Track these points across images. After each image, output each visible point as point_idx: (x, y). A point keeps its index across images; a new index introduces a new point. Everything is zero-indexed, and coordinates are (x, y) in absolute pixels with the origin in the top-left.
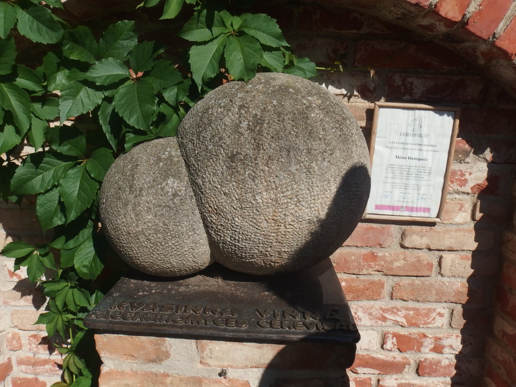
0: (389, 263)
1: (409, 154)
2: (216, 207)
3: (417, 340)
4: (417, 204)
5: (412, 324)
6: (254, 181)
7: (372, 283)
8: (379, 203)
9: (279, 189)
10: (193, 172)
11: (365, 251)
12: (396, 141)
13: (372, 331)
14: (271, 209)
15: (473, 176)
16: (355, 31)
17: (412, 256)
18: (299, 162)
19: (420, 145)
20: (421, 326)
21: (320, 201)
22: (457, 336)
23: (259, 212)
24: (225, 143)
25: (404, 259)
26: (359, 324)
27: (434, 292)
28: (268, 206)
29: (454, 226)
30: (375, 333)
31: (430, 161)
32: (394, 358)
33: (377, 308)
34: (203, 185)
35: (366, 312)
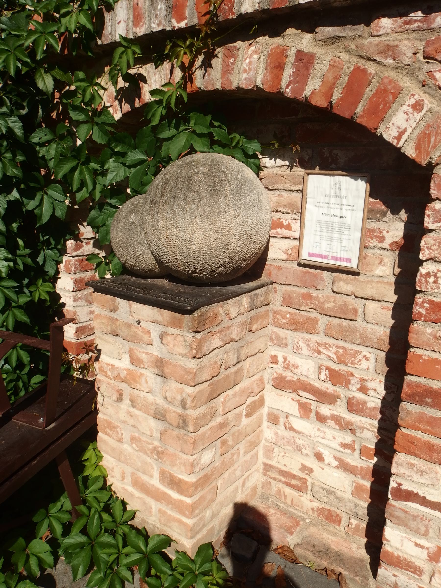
1: (332, 212)
3: (345, 377)
5: (340, 362)
7: (309, 318)
8: (311, 252)
15: (390, 234)
16: (294, 117)
18: (179, 204)
19: (341, 205)
20: (349, 365)
22: (380, 382)
25: (334, 302)
29: (376, 278)
31: (349, 218)
32: (327, 389)
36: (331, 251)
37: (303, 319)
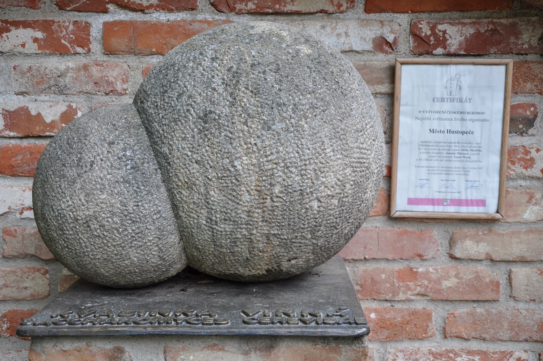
0: (435, 282)
2: (186, 180)
4: (466, 194)
6: (231, 144)
7: (414, 313)
8: (412, 196)
9: (262, 152)
11: (398, 266)
12: (428, 109)
14: (253, 177)
17: (467, 272)
19: (462, 113)
21: (313, 166)
23: (238, 181)
24: (195, 102)
25: (456, 276)
27: (506, 325)
28: (249, 173)
29: (524, 226)
31: (477, 133)
33: (425, 352)
34: (170, 154)
36: (449, 190)
37: (403, 317)
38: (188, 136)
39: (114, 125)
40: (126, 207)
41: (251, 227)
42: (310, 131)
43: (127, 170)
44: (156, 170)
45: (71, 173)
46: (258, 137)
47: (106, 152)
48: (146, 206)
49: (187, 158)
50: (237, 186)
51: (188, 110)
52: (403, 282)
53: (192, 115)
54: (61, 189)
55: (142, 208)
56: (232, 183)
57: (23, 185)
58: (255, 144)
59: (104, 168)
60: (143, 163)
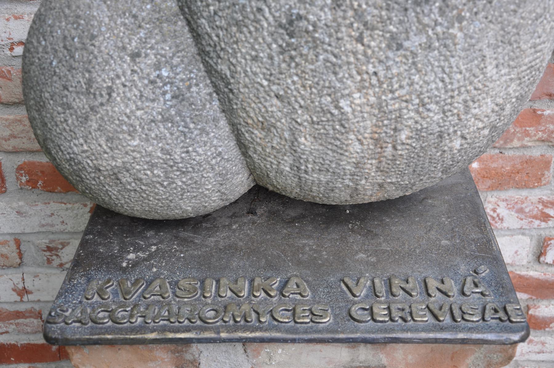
2: (260, 119)
6: (335, 73)
7: (529, 161)
10: (208, 49)
13: (520, 236)
21: (463, 97)
23: (345, 127)
26: (499, 227)
28: (363, 117)
30: (527, 240)
33: (534, 201)
35: (513, 207)
38: (261, 55)
39: (135, 17)
40: (170, 155)
41: (358, 178)
42: (466, 42)
43: (165, 101)
44: (210, 94)
45: (81, 103)
46: (380, 61)
47: (129, 72)
48: (200, 150)
49: (262, 89)
50: (342, 134)
51: (260, 10)
52: (521, 127)
53: (266, 19)
54: (67, 125)
55: (194, 154)
56: (334, 129)
57: (5, 11)
58: (375, 73)
59: (129, 99)
60: (189, 87)
